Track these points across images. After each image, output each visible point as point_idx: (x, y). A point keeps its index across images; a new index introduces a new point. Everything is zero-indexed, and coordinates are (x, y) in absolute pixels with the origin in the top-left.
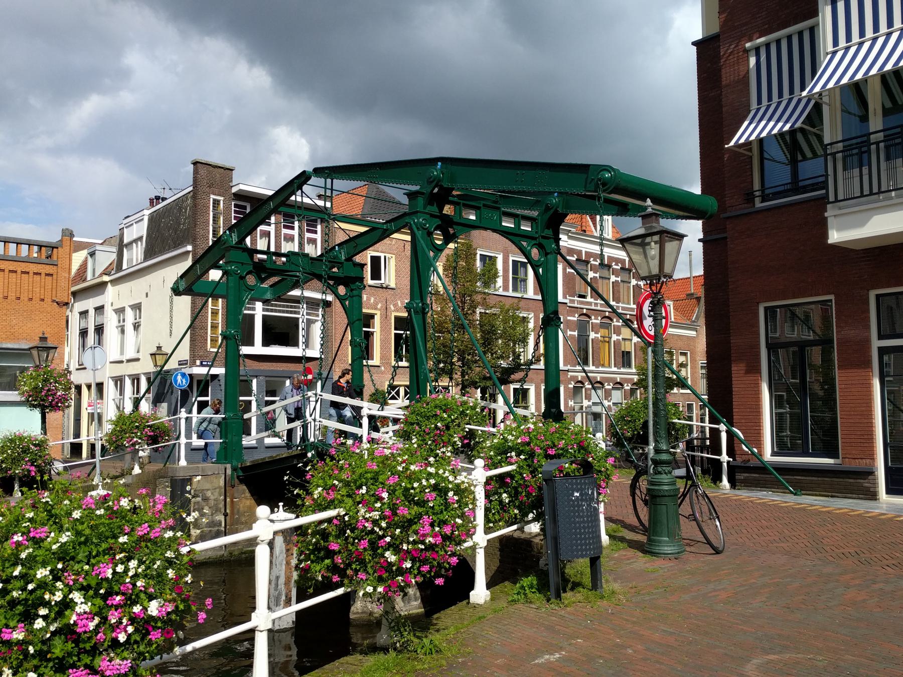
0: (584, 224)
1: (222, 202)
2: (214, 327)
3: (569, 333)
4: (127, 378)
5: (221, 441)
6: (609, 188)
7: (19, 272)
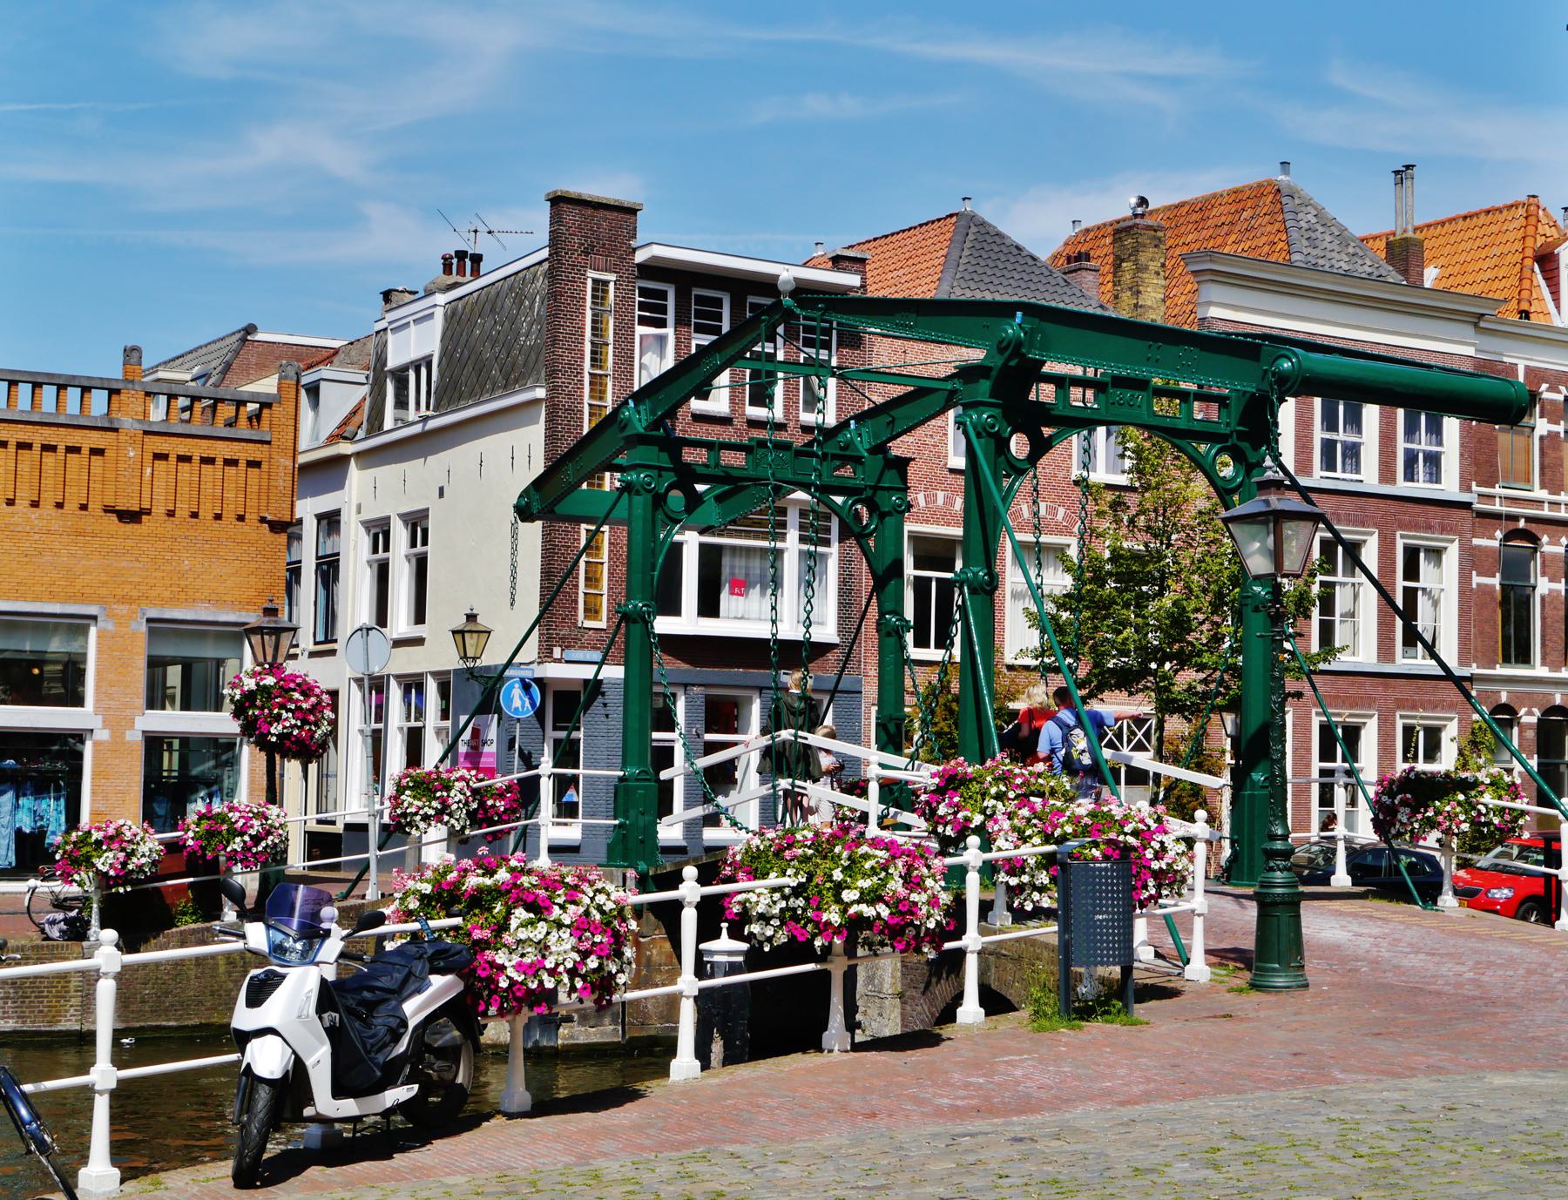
0: (1525, 294)
2: (592, 580)
3: (1477, 580)
5: (617, 822)
6: (1294, 383)
7: (196, 459)
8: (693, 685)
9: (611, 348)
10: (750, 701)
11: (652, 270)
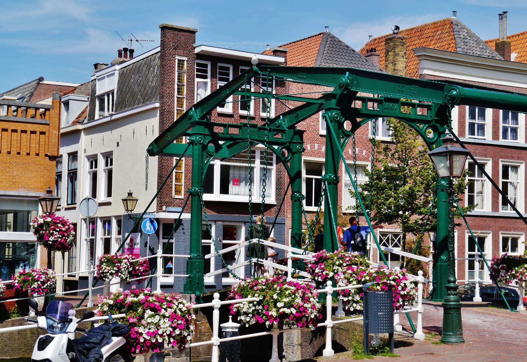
1: (185, 62)
2: (178, 179)
4: (99, 220)
5: (188, 276)
7: (19, 131)
8: (218, 221)
9: (185, 87)
10: (241, 227)
11: (202, 56)
